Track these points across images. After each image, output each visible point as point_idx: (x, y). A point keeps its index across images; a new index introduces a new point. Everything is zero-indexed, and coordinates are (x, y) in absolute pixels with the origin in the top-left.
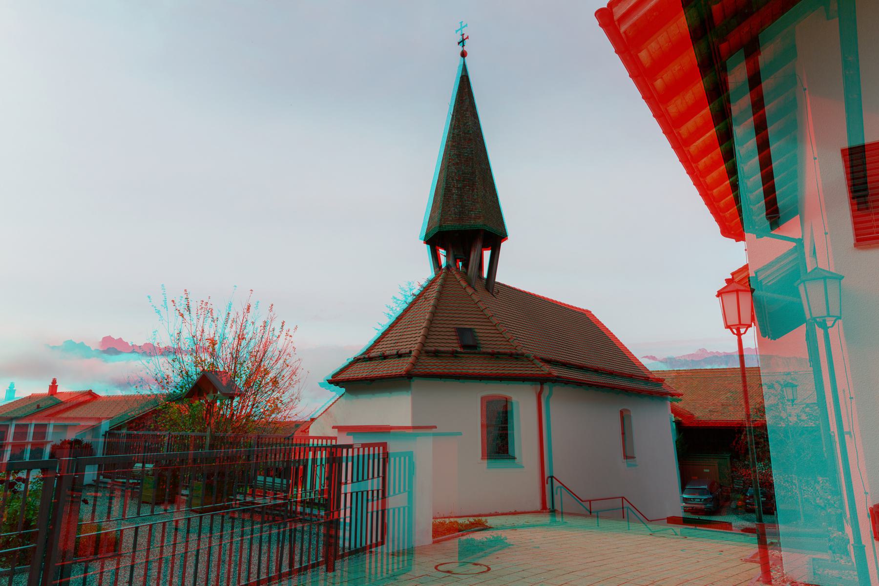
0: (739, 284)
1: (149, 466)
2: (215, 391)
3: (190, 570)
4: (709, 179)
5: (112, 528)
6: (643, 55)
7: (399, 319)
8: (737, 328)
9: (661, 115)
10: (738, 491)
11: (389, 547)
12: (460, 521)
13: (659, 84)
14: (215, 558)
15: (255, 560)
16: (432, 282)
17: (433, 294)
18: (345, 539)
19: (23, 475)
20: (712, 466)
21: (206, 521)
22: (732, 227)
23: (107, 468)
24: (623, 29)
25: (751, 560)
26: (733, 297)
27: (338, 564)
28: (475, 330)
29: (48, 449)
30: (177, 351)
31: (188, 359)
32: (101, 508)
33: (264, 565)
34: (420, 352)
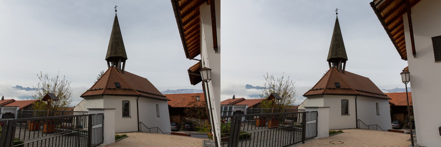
0: (406, 72)
1: (258, 117)
2: (50, 99)
3: (268, 143)
4: (398, 45)
5: (249, 132)
6: (382, 14)
7: (321, 80)
8: (405, 82)
9: (386, 29)
10: (406, 123)
11: (318, 137)
12: (336, 131)
13: (386, 21)
14: (274, 140)
15: (284, 141)
16: (329, 71)
17: (329, 74)
18: (307, 136)
19: (226, 119)
20: (401, 117)
21: (272, 131)
22: (404, 57)
23: (247, 118)
24: (377, 7)
25: (409, 140)
26: (405, 74)
27: (305, 141)
28: (340, 83)
29: (232, 113)
30: (265, 88)
31: (268, 90)
32: (246, 128)
33: (287, 142)
34: (326, 88)
